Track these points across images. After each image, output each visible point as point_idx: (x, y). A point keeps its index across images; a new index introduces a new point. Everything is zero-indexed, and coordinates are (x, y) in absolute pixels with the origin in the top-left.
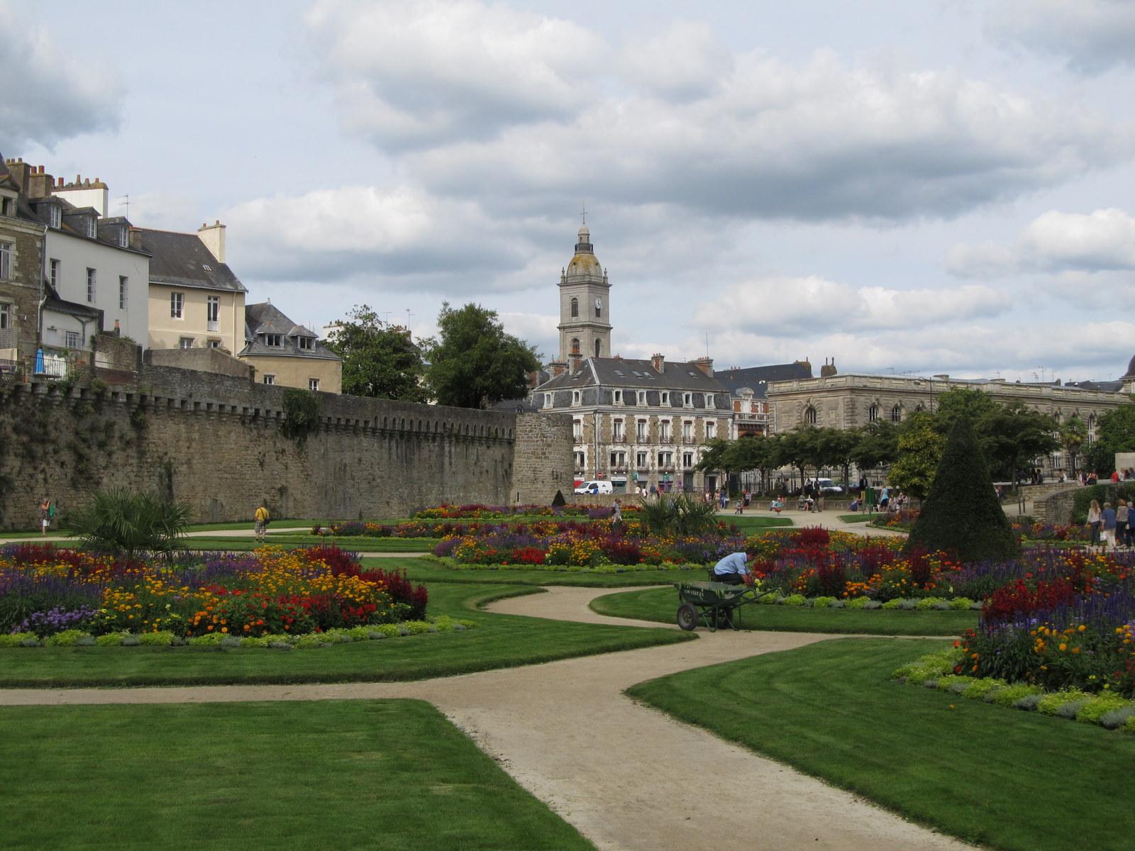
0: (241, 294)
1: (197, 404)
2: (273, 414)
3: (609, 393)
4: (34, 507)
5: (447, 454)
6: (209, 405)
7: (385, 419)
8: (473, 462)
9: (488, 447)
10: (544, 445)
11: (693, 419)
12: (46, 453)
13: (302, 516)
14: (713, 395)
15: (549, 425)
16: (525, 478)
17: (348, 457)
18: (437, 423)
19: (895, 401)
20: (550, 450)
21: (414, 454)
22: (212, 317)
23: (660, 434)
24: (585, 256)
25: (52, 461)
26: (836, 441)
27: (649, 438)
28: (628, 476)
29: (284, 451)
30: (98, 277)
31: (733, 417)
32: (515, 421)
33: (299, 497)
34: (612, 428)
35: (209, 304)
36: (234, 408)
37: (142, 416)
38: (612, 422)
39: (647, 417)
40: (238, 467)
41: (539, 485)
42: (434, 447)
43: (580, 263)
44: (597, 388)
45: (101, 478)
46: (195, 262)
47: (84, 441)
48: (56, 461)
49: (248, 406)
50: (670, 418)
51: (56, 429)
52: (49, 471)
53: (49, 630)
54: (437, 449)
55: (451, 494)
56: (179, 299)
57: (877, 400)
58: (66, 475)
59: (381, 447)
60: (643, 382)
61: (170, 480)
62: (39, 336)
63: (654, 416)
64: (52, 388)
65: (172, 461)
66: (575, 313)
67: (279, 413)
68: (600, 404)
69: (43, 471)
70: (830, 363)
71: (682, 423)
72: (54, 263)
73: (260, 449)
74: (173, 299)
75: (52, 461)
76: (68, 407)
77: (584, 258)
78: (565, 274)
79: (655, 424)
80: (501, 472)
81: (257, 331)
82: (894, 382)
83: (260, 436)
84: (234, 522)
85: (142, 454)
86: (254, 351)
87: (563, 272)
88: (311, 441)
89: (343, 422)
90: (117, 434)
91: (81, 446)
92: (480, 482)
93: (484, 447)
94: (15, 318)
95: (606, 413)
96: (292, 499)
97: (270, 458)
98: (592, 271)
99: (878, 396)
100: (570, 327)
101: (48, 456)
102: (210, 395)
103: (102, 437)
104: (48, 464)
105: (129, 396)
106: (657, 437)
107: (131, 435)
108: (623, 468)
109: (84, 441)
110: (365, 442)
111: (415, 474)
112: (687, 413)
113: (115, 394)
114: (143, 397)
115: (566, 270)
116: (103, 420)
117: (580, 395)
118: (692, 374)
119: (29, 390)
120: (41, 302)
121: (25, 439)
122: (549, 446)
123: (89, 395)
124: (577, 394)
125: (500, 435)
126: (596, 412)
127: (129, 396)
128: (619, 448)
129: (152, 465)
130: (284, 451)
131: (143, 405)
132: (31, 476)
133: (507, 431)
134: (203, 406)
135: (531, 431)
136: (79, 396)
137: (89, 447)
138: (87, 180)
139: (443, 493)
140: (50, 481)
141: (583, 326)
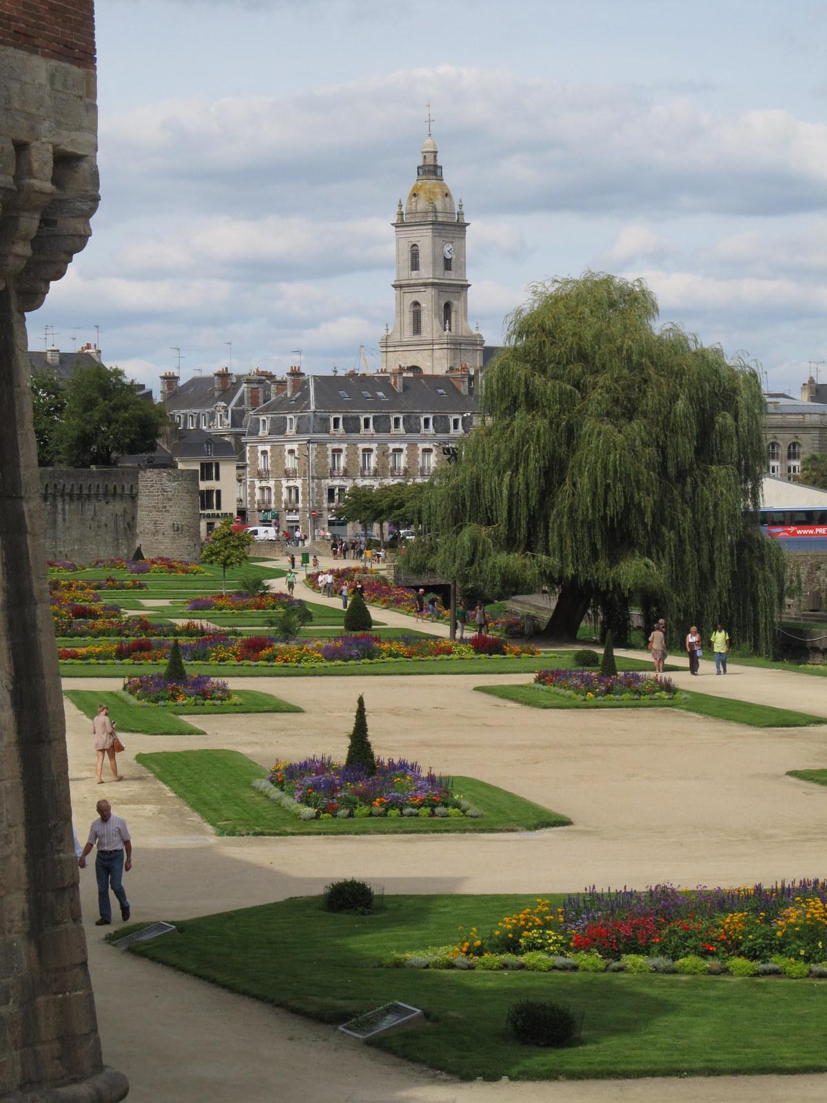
3: (327, 420)
8: (90, 517)
9: (107, 503)
15: (170, 481)
23: (391, 465)
24: (430, 183)
26: (399, 501)
27: (376, 471)
32: (137, 477)
34: (330, 460)
38: (330, 453)
39: (374, 446)
41: (160, 537)
43: (422, 194)
44: (312, 414)
50: (404, 446)
54: (49, 507)
55: (65, 547)
60: (375, 404)
66: (415, 266)
68: (314, 432)
71: (420, 452)
77: (427, 187)
79: (383, 454)
80: (122, 525)
87: (401, 206)
92: (97, 535)
93: (101, 504)
95: (321, 444)
98: (439, 205)
100: (409, 286)
106: (386, 468)
115: (404, 203)
117: (295, 422)
118: (441, 391)
122: (170, 500)
125: (119, 491)
126: (309, 442)
128: (337, 482)
133: (127, 487)
135: (152, 486)
139: (55, 547)
141: (425, 285)
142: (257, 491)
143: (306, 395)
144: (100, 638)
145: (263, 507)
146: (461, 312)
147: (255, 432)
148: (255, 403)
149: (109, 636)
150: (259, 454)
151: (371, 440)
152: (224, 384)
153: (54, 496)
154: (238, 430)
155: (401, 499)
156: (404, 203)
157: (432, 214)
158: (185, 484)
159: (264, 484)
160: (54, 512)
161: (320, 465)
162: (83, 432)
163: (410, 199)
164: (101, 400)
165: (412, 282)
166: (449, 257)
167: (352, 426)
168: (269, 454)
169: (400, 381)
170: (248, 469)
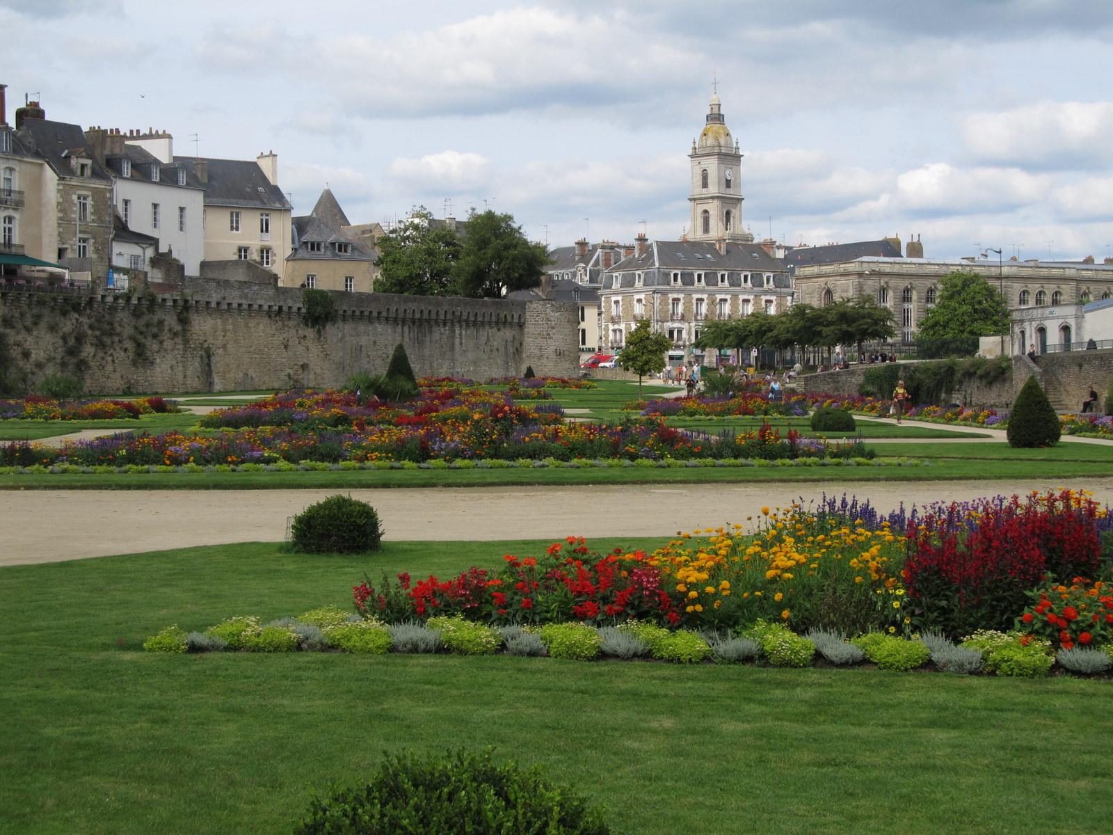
0: (288, 210)
1: (229, 304)
2: (295, 309)
3: (669, 275)
4: (105, 379)
5: (457, 336)
6: (240, 305)
7: (397, 310)
9: (499, 330)
10: (548, 328)
11: (751, 297)
12: (113, 343)
13: (321, 386)
14: (772, 275)
15: (553, 311)
16: (533, 355)
17: (364, 341)
18: (446, 312)
19: (906, 283)
20: (554, 331)
21: (425, 337)
22: (265, 228)
23: (718, 312)
24: (716, 126)
25: (118, 348)
28: (686, 350)
29: (305, 337)
30: (161, 209)
31: (792, 295)
32: (525, 308)
33: (319, 371)
34: (671, 307)
35: (262, 220)
36: (260, 306)
37: (185, 314)
38: (670, 301)
39: (705, 296)
40: (266, 349)
41: (544, 361)
42: (446, 331)
43: (710, 134)
44: (656, 271)
45: (155, 359)
46: (251, 186)
47: (141, 333)
48: (121, 348)
49: (273, 304)
50: (728, 297)
51: (120, 326)
52: (116, 355)
53: (7, 418)
56: (237, 216)
57: (886, 283)
58: (128, 357)
59: (395, 332)
60: (704, 263)
61: (209, 360)
62: (110, 260)
63: (711, 295)
64: (116, 298)
65: (211, 346)
66: (705, 185)
67: (299, 309)
68: (658, 285)
69: (111, 355)
70: (915, 240)
71: (740, 302)
72: (126, 202)
73: (284, 336)
74: (232, 216)
75: (118, 348)
76: (129, 310)
77: (714, 129)
78: (697, 146)
80: (511, 350)
81: (304, 239)
82: (904, 266)
83: (284, 326)
84: (263, 390)
85: (186, 342)
86: (298, 256)
87: (694, 143)
88: (331, 331)
89: (357, 313)
90: (167, 328)
91: (139, 337)
92: (490, 358)
94: (92, 248)
95: (664, 293)
96: (313, 373)
97: (294, 342)
98: (722, 142)
99: (886, 280)
101: (115, 345)
102: (241, 297)
103: (155, 330)
104: (115, 350)
105: (175, 301)
107: (178, 328)
108: (681, 343)
109: (141, 333)
110: (380, 328)
111: (427, 352)
112: (745, 291)
113: (164, 300)
114: (186, 301)
116: (155, 319)
118: (755, 255)
119: (99, 299)
120: (111, 236)
121: (98, 333)
122: (553, 328)
123: (144, 302)
124: (639, 275)
125: (509, 319)
126: (654, 292)
127: (175, 301)
128: (676, 325)
129: (195, 349)
130: (305, 337)
131: (186, 307)
132: (103, 358)
133: (516, 317)
134: (235, 306)
135: (538, 316)
136: (136, 302)
137: (145, 338)
138: (157, 131)
139: (453, 368)
140: (117, 361)
141: (713, 198)
142: (611, 333)
143: (651, 255)
144: (575, 461)
145: (615, 345)
146: (737, 216)
147: (608, 286)
148: (607, 265)
149: (595, 458)
150: (613, 303)
151: (703, 291)
152: (583, 250)
153: (452, 322)
154: (594, 285)
155: (769, 323)
156: (697, 141)
157: (718, 148)
158: (566, 314)
159: (616, 327)
160: (452, 337)
161: (663, 311)
162: (478, 267)
163: (701, 137)
164: (493, 239)
165: (703, 196)
166: (729, 178)
167: (688, 280)
168: (621, 303)
169: (723, 246)
170: (603, 316)
